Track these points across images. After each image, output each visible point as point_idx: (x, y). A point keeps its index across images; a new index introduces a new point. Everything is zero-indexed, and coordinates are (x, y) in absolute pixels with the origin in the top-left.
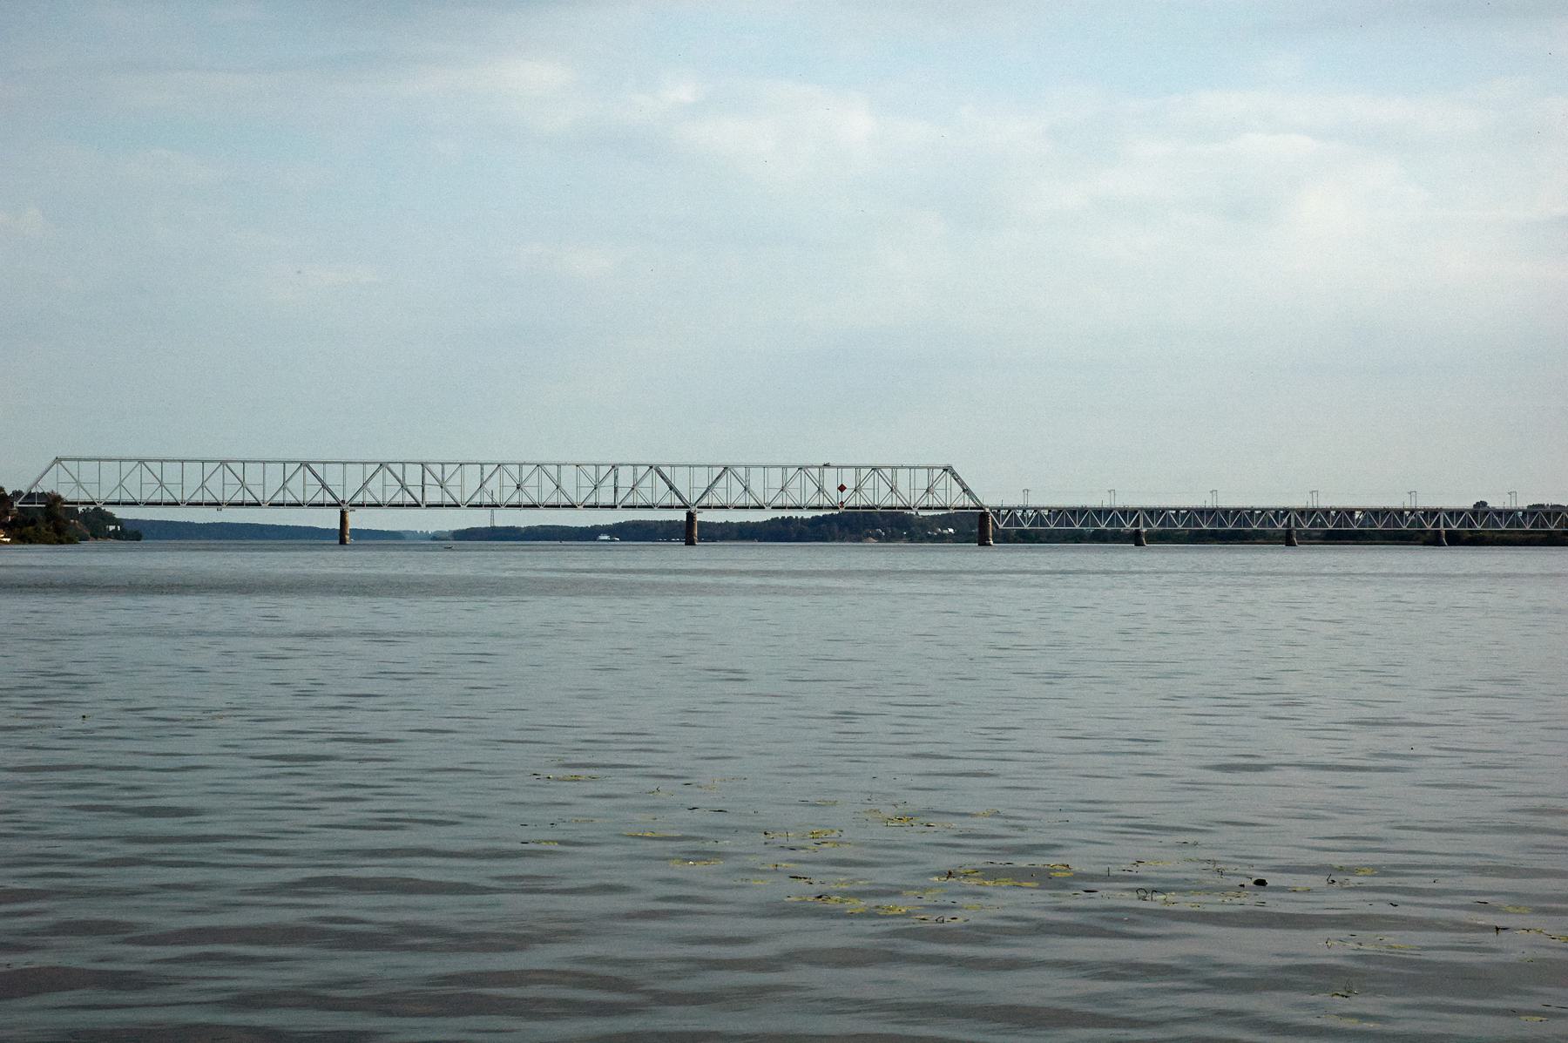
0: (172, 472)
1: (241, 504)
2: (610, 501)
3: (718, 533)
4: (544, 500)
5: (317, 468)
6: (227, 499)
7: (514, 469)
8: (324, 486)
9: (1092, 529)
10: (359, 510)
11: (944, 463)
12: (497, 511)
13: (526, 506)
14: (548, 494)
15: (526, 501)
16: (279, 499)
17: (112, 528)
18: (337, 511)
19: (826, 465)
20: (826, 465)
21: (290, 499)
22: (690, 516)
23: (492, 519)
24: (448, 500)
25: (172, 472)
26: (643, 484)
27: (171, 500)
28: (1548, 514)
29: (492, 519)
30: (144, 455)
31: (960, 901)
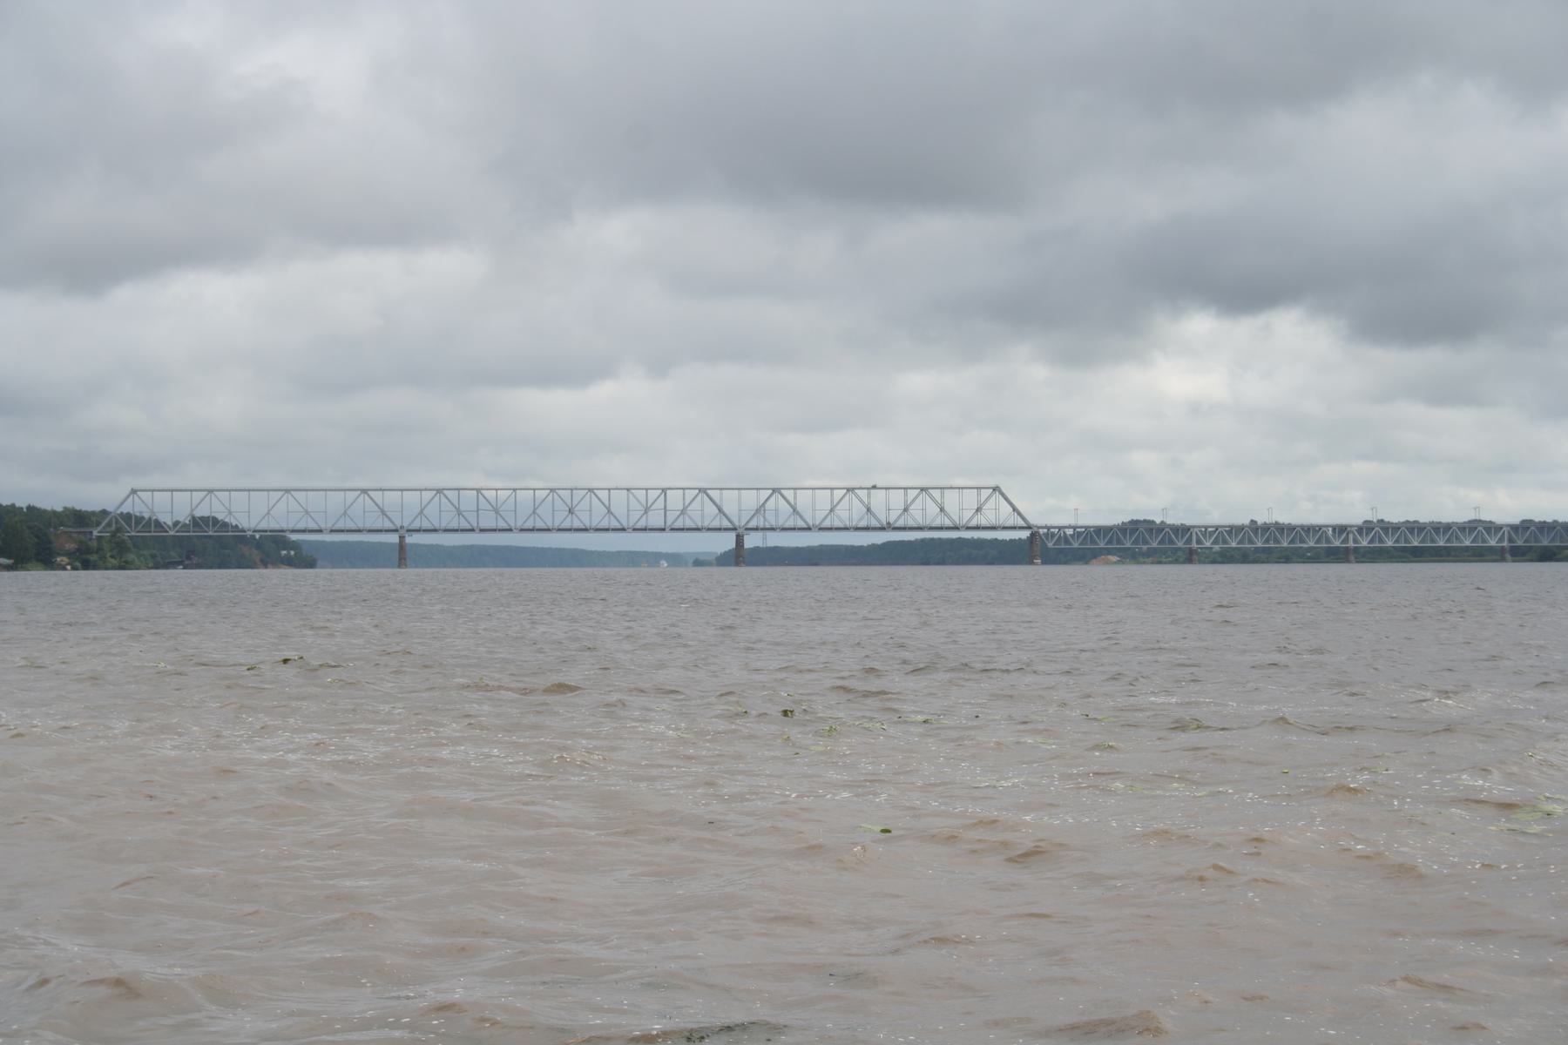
0: (878, 498)
1: (645, 529)
2: (661, 525)
3: (174, 555)
4: (1001, 522)
5: (714, 494)
6: (519, 524)
7: (566, 494)
8: (720, 510)
9: (1145, 547)
10: (753, 534)
11: (993, 484)
12: (769, 534)
13: (615, 530)
14: (561, 519)
15: (577, 524)
16: (529, 525)
17: (284, 552)
18: (733, 535)
19: (874, 487)
20: (874, 487)
21: (689, 524)
22: (740, 540)
23: (765, 538)
24: (502, 525)
25: (878, 498)
26: (693, 506)
27: (468, 526)
28: (1386, 530)
29: (765, 538)
30: (440, 485)
31: (722, 725)
